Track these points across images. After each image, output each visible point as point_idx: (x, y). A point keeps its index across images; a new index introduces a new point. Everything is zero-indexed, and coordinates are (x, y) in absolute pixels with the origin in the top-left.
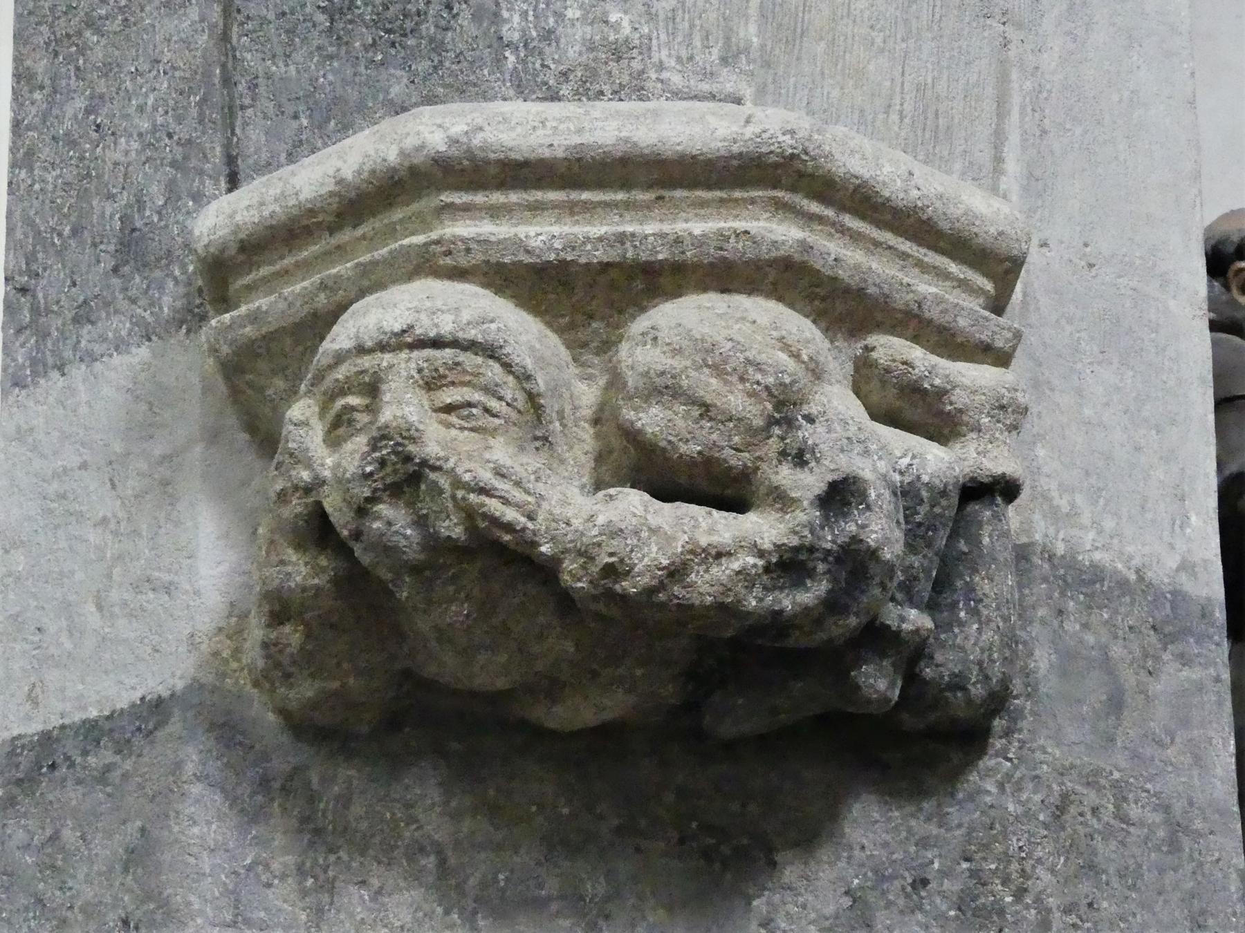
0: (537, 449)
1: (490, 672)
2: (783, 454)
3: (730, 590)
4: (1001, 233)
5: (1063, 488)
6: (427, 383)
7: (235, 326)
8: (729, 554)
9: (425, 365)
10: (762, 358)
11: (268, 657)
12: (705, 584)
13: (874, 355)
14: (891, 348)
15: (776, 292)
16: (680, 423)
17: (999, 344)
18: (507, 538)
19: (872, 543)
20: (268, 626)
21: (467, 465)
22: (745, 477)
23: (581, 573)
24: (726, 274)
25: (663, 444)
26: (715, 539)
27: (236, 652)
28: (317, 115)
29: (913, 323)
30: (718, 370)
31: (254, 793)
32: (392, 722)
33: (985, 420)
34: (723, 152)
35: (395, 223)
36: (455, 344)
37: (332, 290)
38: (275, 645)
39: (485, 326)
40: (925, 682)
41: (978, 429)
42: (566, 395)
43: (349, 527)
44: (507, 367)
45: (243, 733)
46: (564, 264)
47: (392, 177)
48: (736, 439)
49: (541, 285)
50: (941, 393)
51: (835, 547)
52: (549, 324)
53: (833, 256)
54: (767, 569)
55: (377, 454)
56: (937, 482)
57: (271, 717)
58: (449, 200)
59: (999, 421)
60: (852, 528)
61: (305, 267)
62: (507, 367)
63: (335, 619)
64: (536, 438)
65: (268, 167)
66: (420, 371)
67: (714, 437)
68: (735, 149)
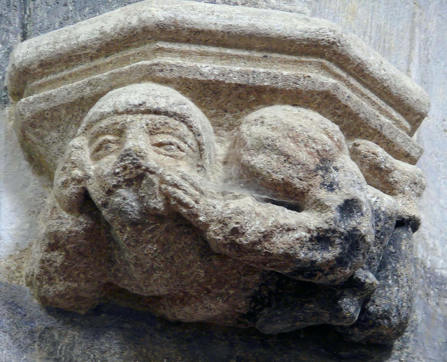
0: (198, 171)
1: (159, 285)
2: (323, 184)
3: (292, 247)
4: (418, 100)
5: (431, 236)
6: (150, 131)
7: (35, 103)
8: (294, 230)
9: (150, 122)
10: (316, 136)
11: (42, 268)
12: (280, 243)
13: (359, 148)
14: (367, 146)
15: (318, 109)
16: (274, 163)
17: (413, 154)
18: (185, 210)
19: (363, 232)
20: (46, 251)
21: (168, 173)
22: (303, 194)
23: (220, 231)
24: (296, 97)
25: (265, 173)
26: (287, 222)
27: (19, 269)
28: (78, 5)
29: (377, 136)
30: (295, 139)
31: (25, 338)
32: (97, 311)
33: (407, 188)
34: (299, 37)
35: (130, 56)
36: (166, 113)
37: (94, 86)
38: (48, 261)
39: (181, 106)
40: (369, 314)
41: (403, 192)
42: (212, 148)
43: (102, 200)
44: (190, 127)
45: (20, 308)
46: (218, 83)
47: (133, 32)
48: (301, 174)
49: (206, 92)
50: (389, 172)
51: (345, 232)
52: (205, 113)
53: (347, 95)
54: (311, 240)
55: (123, 163)
56: (388, 211)
57: (35, 301)
58: (161, 46)
59: (413, 190)
60: (353, 223)
61: (76, 76)
62: (190, 127)
63: (82, 249)
64: (198, 166)
65: (43, 30)
66: (147, 125)
67: (291, 172)
68: (306, 36)
